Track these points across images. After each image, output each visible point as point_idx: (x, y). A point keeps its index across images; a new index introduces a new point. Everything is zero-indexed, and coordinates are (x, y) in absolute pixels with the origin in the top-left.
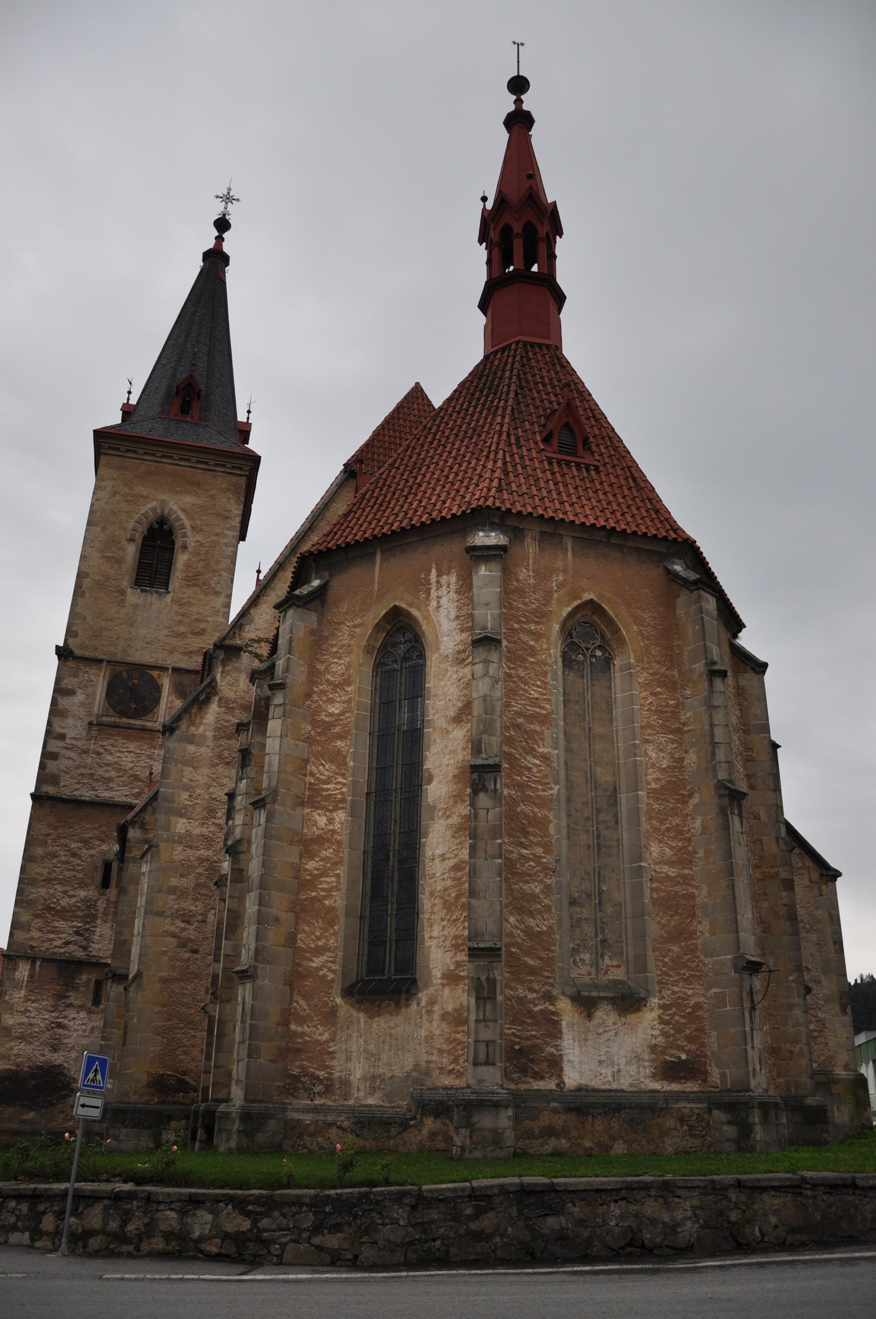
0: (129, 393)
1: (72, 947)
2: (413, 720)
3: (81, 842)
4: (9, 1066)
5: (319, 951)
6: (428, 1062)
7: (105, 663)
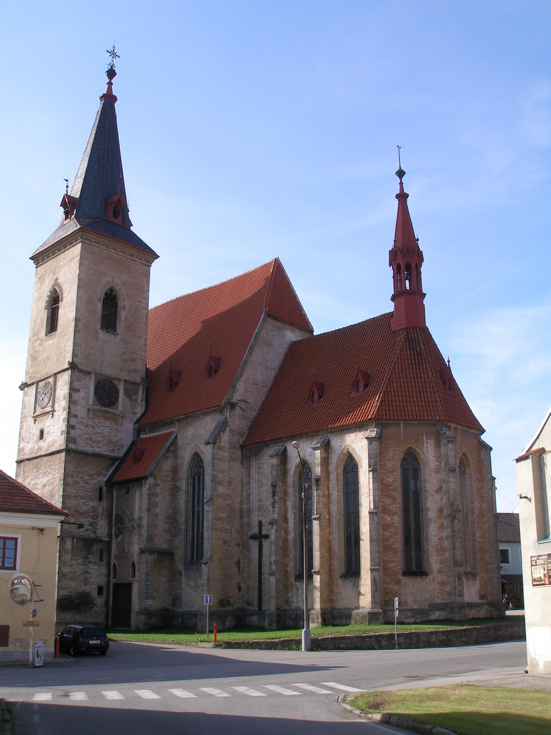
0: (67, 187)
1: (89, 532)
2: (416, 487)
3: (89, 476)
4: (67, 593)
5: (392, 562)
6: (434, 596)
7: (93, 376)
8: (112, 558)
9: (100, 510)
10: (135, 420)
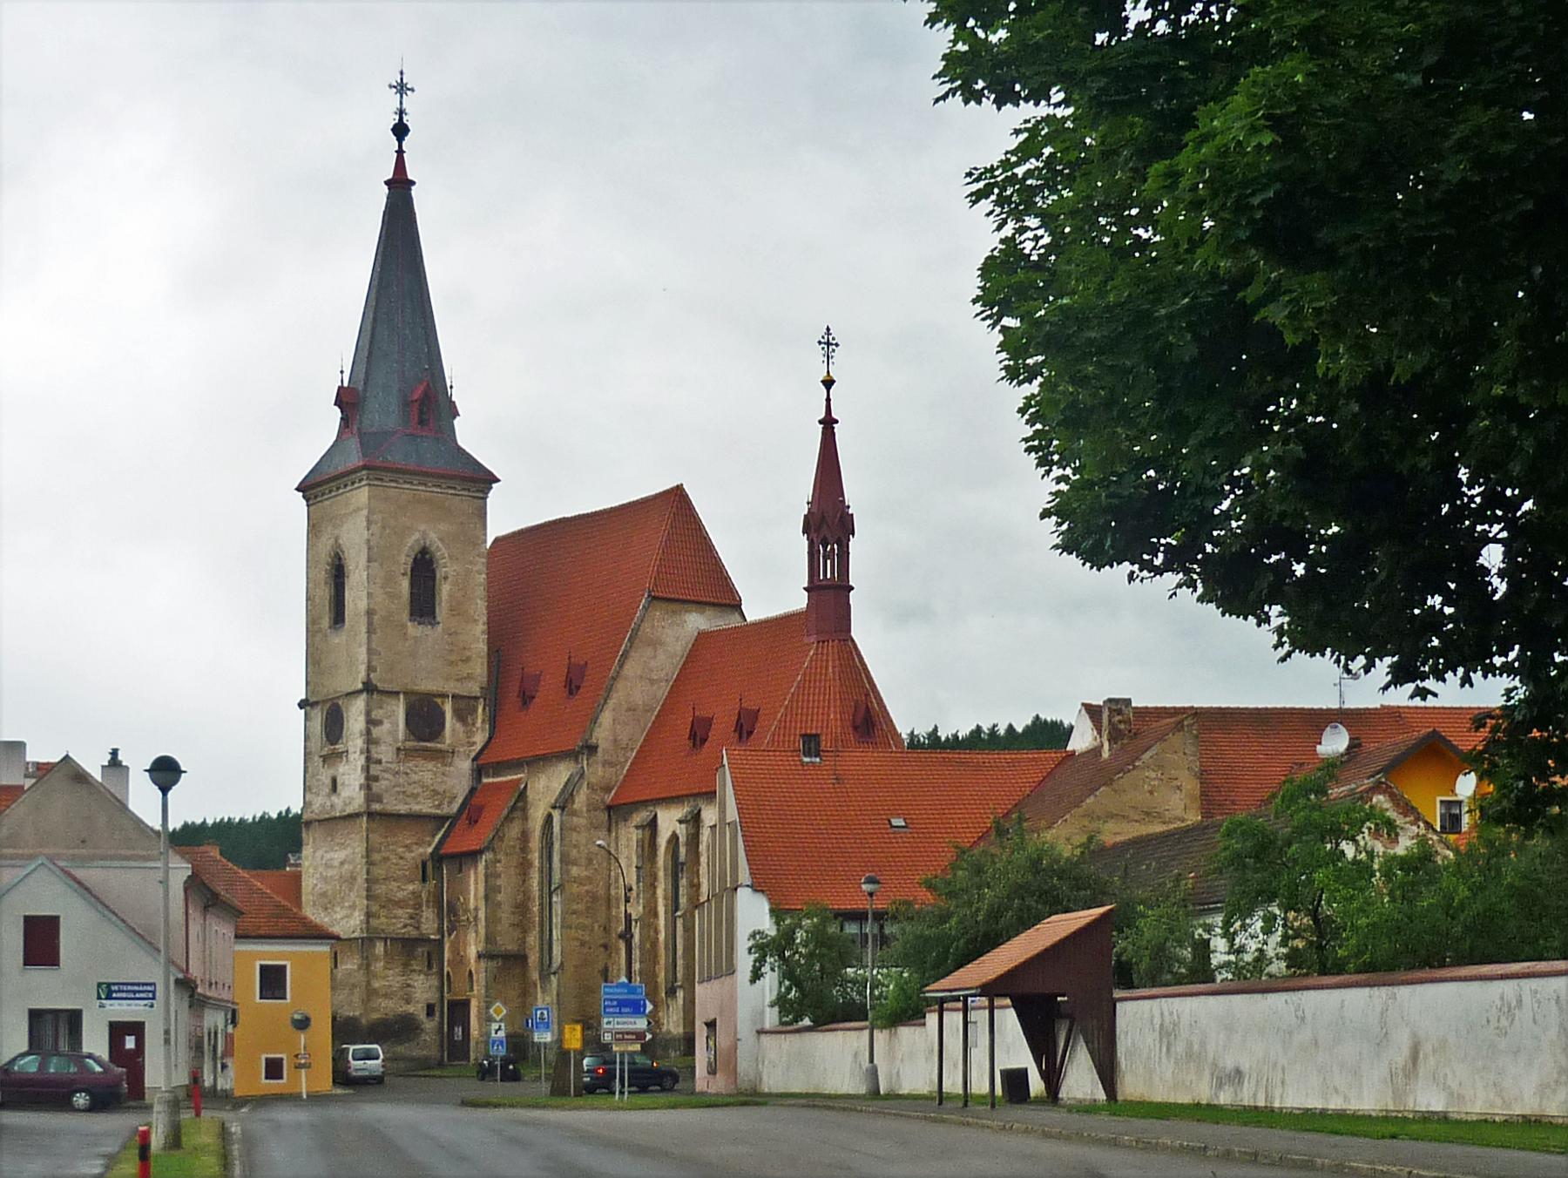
0: (342, 372)
7: (402, 696)
8: (446, 964)
9: (424, 895)
10: (473, 755)
